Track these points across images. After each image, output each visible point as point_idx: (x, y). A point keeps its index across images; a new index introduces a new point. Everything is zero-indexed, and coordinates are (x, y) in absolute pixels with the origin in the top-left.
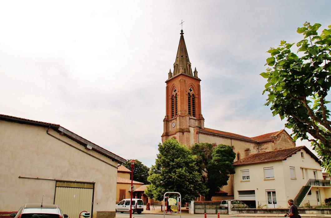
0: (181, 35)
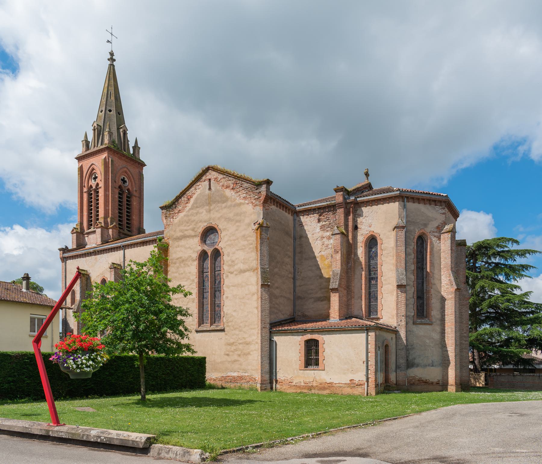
0: (109, 62)
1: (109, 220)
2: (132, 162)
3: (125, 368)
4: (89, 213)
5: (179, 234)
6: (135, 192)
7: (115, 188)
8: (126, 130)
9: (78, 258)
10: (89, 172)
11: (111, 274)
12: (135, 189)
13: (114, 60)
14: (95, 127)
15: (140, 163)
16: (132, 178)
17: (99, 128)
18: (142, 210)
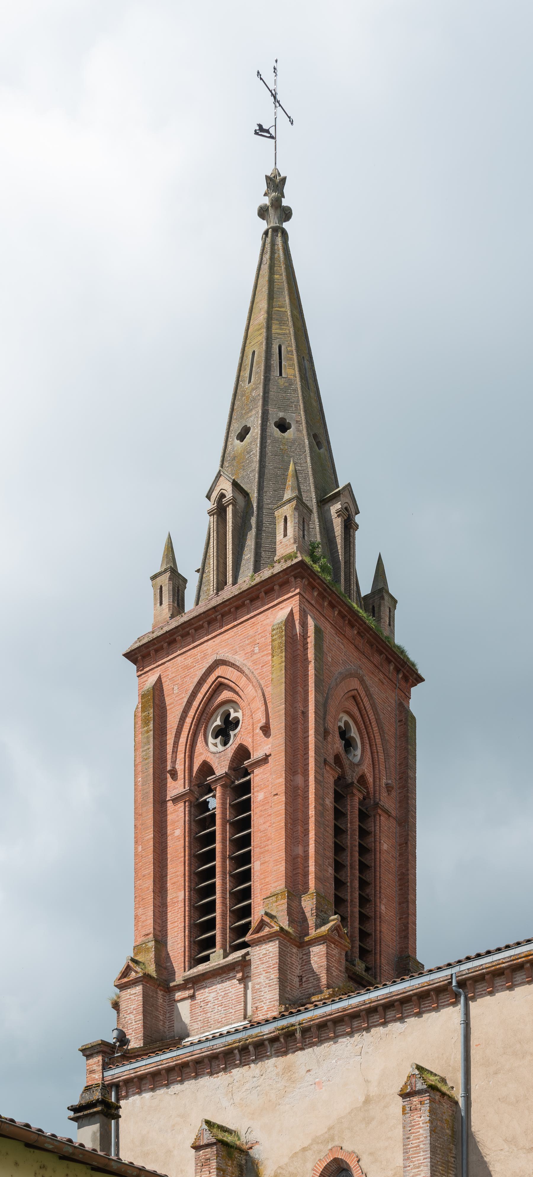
0: (263, 225)
1: (308, 904)
2: (377, 659)
6: (384, 794)
8: (353, 510)
9: (182, 1082)
10: (196, 704)
11: (408, 1129)
12: (384, 781)
14: (223, 496)
17: (240, 499)
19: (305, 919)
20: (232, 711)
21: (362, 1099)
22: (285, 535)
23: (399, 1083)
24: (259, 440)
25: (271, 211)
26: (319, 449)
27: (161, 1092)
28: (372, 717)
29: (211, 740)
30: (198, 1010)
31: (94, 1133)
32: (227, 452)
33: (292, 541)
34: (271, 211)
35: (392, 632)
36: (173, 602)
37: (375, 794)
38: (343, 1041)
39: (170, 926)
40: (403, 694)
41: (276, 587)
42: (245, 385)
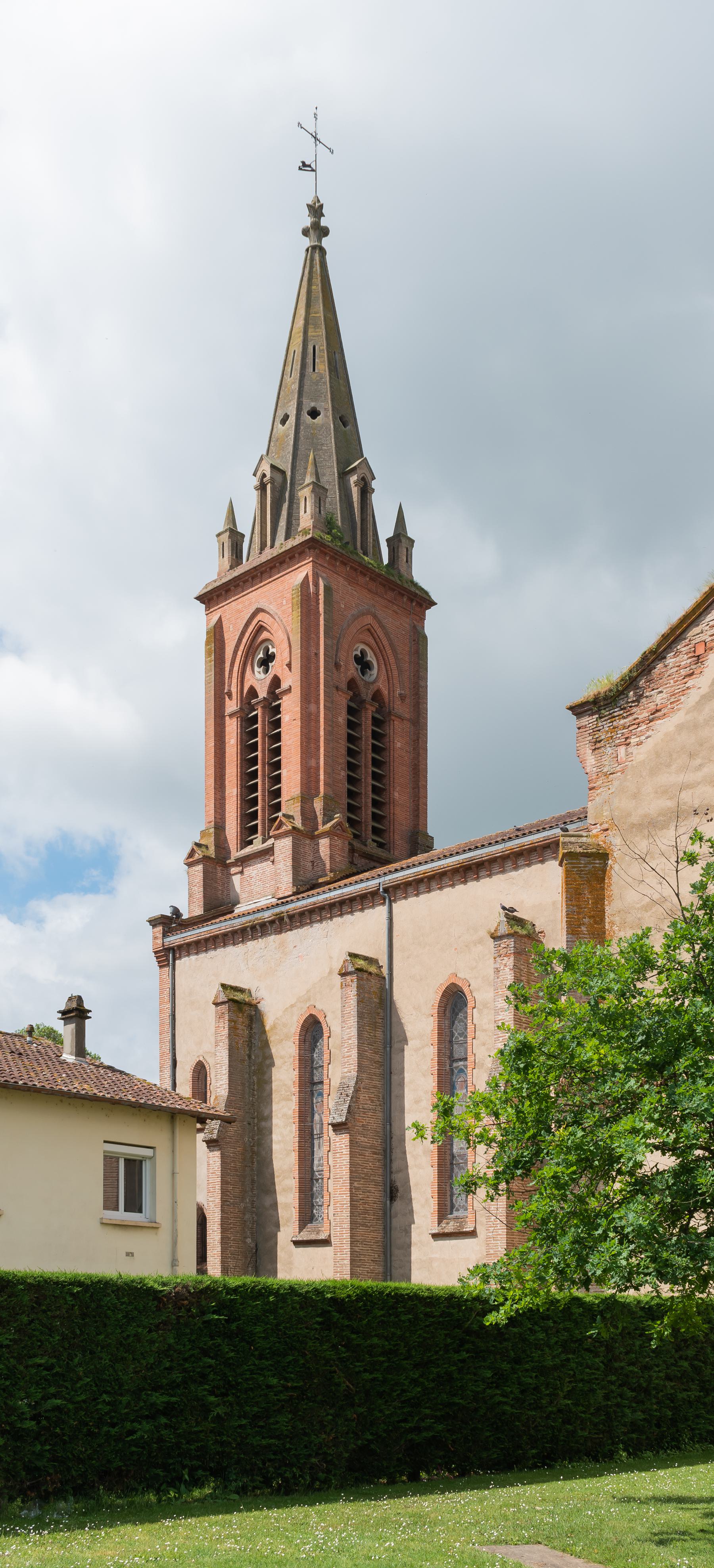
0: (306, 242)
1: (318, 805)
2: (390, 595)
3: (547, 1350)
4: (248, 789)
5: (654, 805)
6: (398, 702)
7: (337, 688)
8: (369, 477)
9: (215, 949)
10: (244, 640)
11: (344, 999)
12: (398, 692)
13: (325, 232)
14: (264, 476)
15: (416, 595)
16: (389, 652)
17: (278, 477)
18: (421, 767)
19: (316, 817)
20: (270, 647)
21: (327, 970)
22: (305, 512)
23: (337, 965)
24: (293, 428)
25: (311, 231)
26: (345, 427)
27: (202, 956)
28: (385, 642)
29: (256, 669)
30: (246, 883)
31: (72, 1030)
32: (273, 434)
33: (310, 517)
34: (311, 231)
35: (410, 567)
36: (232, 555)
37: (389, 703)
38: (316, 925)
39: (227, 815)
40: (418, 618)
41: (297, 555)
42: (287, 378)
